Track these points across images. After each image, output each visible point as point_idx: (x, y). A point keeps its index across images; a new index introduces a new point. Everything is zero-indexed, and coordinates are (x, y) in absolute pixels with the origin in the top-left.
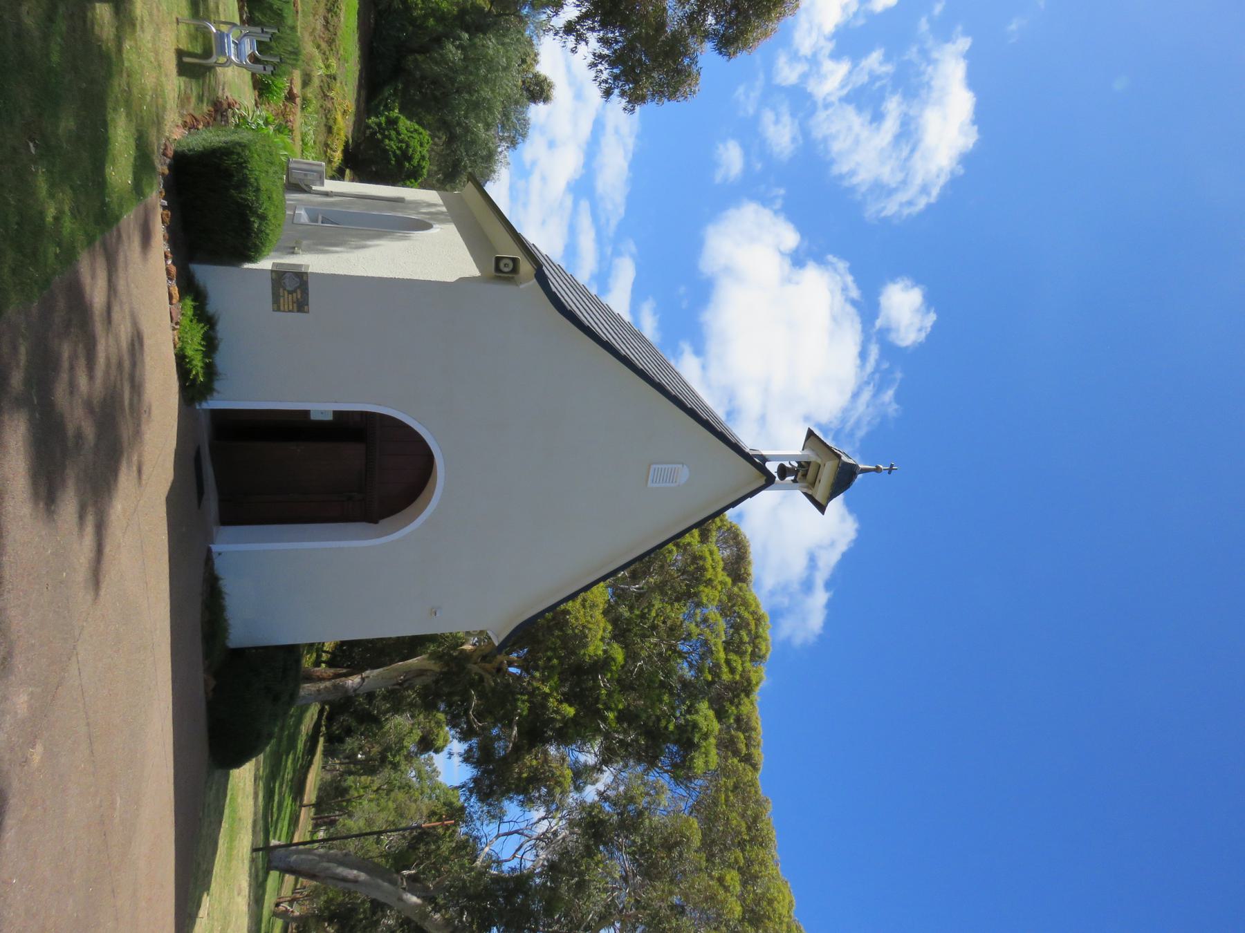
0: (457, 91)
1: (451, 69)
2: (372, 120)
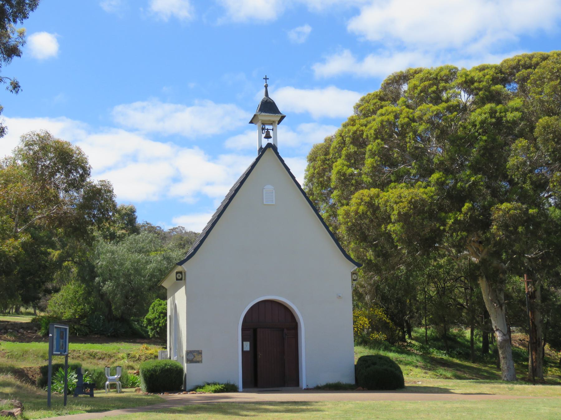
0: (130, 283)
1: (117, 287)
2: (151, 334)
